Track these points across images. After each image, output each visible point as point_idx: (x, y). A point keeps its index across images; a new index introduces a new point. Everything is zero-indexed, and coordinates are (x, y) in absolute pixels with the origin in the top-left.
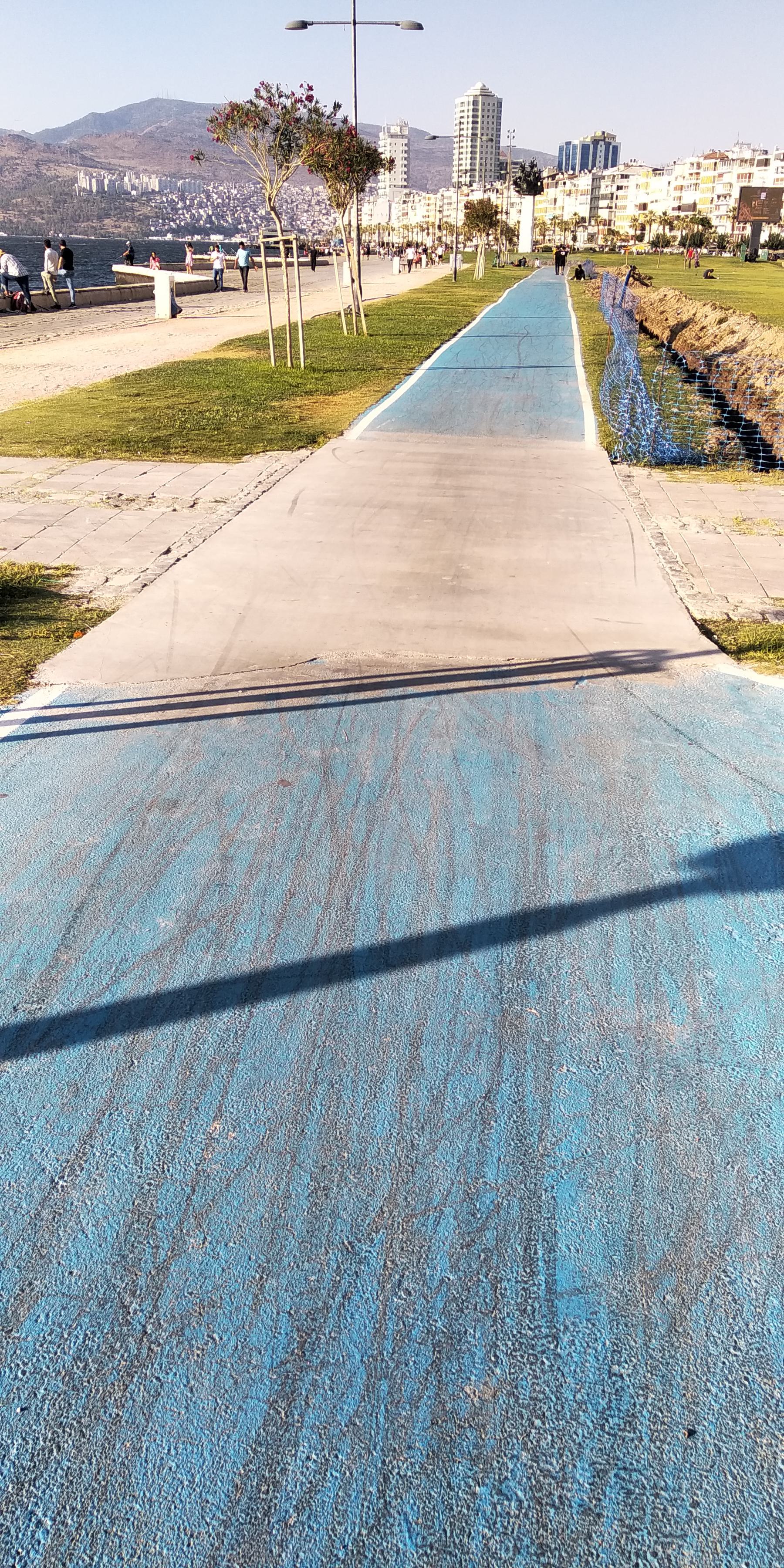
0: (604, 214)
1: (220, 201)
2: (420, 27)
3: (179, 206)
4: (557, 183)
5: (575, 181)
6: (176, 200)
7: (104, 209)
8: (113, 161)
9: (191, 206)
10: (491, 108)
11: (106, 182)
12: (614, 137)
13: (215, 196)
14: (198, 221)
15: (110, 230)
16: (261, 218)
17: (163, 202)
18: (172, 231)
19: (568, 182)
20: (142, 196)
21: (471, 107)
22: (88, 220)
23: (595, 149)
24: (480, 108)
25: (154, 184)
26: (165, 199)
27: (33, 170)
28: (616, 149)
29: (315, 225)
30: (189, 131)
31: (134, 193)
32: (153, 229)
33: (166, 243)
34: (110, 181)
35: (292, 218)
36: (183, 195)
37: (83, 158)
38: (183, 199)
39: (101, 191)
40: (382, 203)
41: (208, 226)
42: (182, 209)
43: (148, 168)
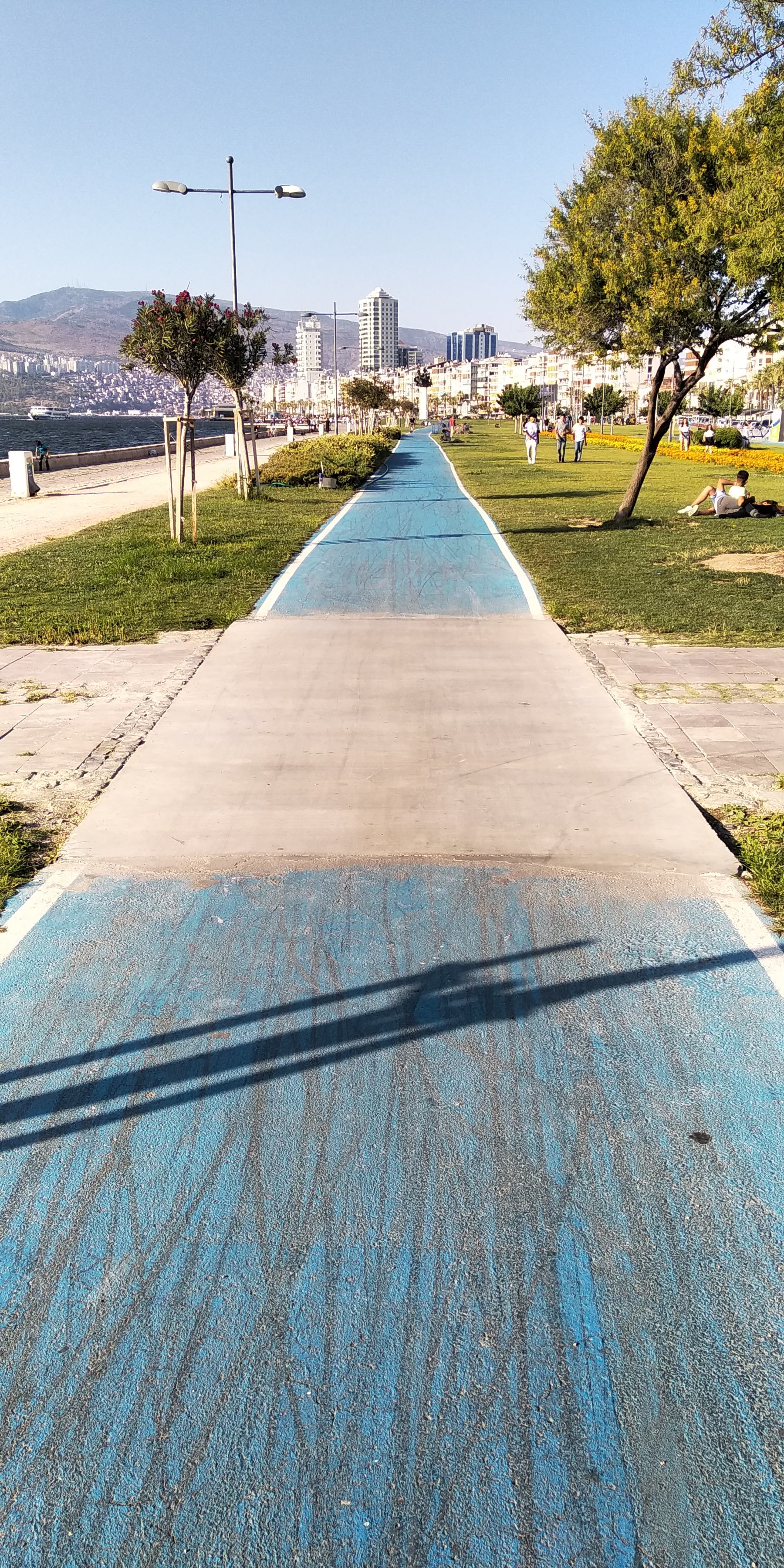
0: (481, 392)
3: (97, 384)
4: (445, 370)
5: (458, 368)
8: (30, 345)
9: (107, 385)
12: (492, 329)
14: (116, 397)
16: (175, 394)
18: (92, 407)
19: (453, 369)
21: (372, 307)
22: (11, 399)
23: (477, 338)
25: (72, 365)
28: (494, 338)
31: (53, 374)
32: (73, 406)
33: (85, 418)
34: (30, 363)
36: (100, 375)
38: (100, 378)
39: (22, 373)
40: (302, 385)
41: (125, 402)
42: (100, 387)
43: (64, 351)
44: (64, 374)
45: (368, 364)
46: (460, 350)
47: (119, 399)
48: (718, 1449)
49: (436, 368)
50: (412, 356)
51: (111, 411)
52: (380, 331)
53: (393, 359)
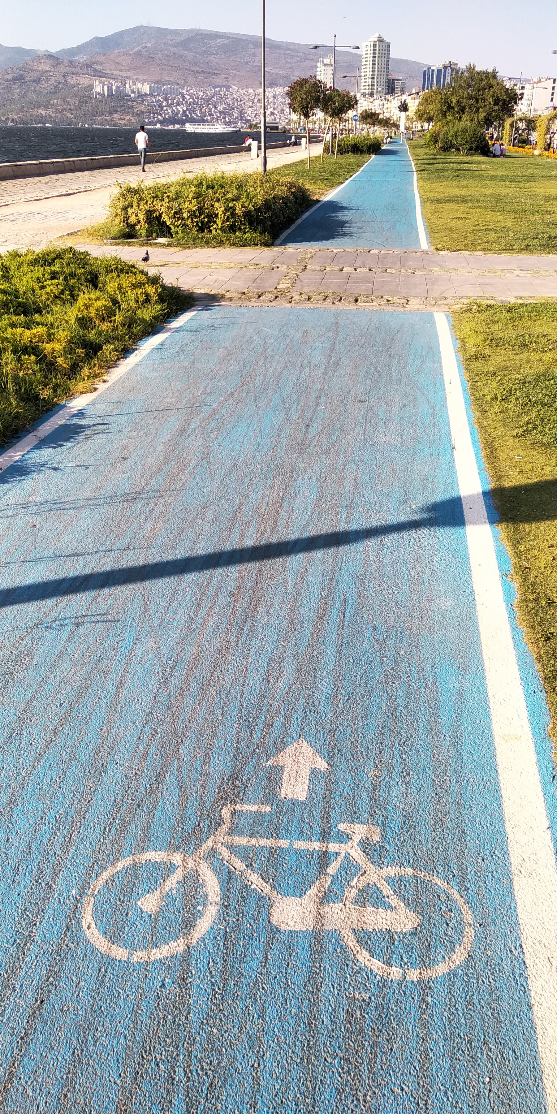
1: (191, 100)
2: (358, 48)
3: (164, 104)
6: (162, 100)
7: (113, 107)
8: (115, 73)
9: (171, 104)
10: (384, 48)
11: (114, 88)
12: (456, 65)
13: (188, 97)
14: (177, 114)
15: (118, 122)
16: (220, 112)
17: (153, 102)
20: (138, 98)
21: (372, 48)
24: (377, 48)
25: (146, 89)
26: (154, 100)
27: (61, 79)
29: (257, 117)
30: (166, 50)
31: (133, 95)
32: (146, 121)
34: (117, 87)
35: (241, 112)
36: (166, 96)
37: (95, 70)
38: (166, 99)
39: (110, 95)
41: (184, 118)
42: (166, 106)
43: (139, 77)
44: (140, 95)
45: (367, 91)
46: (432, 81)
47: (179, 115)
49: (414, 96)
50: (398, 86)
51: (174, 125)
52: (376, 66)
53: (384, 87)
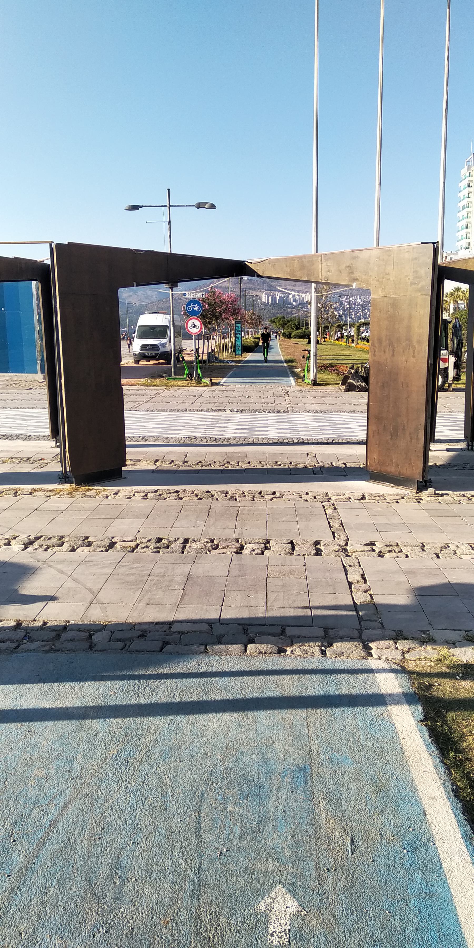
11: (278, 298)
31: (294, 303)
34: (280, 297)
39: (274, 303)
48: (402, 914)
